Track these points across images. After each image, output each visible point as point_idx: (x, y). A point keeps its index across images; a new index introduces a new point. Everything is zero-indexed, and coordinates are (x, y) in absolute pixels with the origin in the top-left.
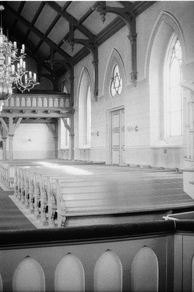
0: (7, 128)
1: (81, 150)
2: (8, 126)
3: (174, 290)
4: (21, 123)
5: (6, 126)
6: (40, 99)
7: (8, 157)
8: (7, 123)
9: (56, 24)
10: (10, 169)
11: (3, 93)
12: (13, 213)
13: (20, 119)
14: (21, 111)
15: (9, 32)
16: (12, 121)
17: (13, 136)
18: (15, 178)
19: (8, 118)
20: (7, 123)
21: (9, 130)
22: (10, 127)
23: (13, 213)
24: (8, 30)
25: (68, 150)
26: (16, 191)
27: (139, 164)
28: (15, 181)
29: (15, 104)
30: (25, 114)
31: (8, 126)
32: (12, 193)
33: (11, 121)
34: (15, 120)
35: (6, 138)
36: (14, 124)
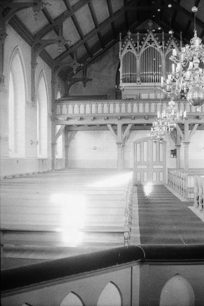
0: (182, 134)
1: (39, 160)
2: (183, 133)
3: (99, 303)
4: (197, 129)
5: (181, 132)
6: (76, 106)
7: (183, 165)
8: (183, 130)
9: (74, 26)
10: (189, 178)
11: (199, 98)
12: (198, 225)
13: (196, 126)
14: (198, 117)
15: (182, 34)
16: (188, 127)
17: (188, 143)
18: (196, 188)
19: (183, 125)
20: (183, 130)
21: (184, 138)
22: (185, 133)
23: (198, 225)
24: (120, 34)
25: (61, 159)
26: (196, 202)
27: (34, 172)
28: (195, 191)
29: (126, 109)
30: (200, 121)
31: (183, 133)
32: (192, 204)
33: (187, 127)
34: (191, 126)
35: (180, 146)
36: (190, 131)
